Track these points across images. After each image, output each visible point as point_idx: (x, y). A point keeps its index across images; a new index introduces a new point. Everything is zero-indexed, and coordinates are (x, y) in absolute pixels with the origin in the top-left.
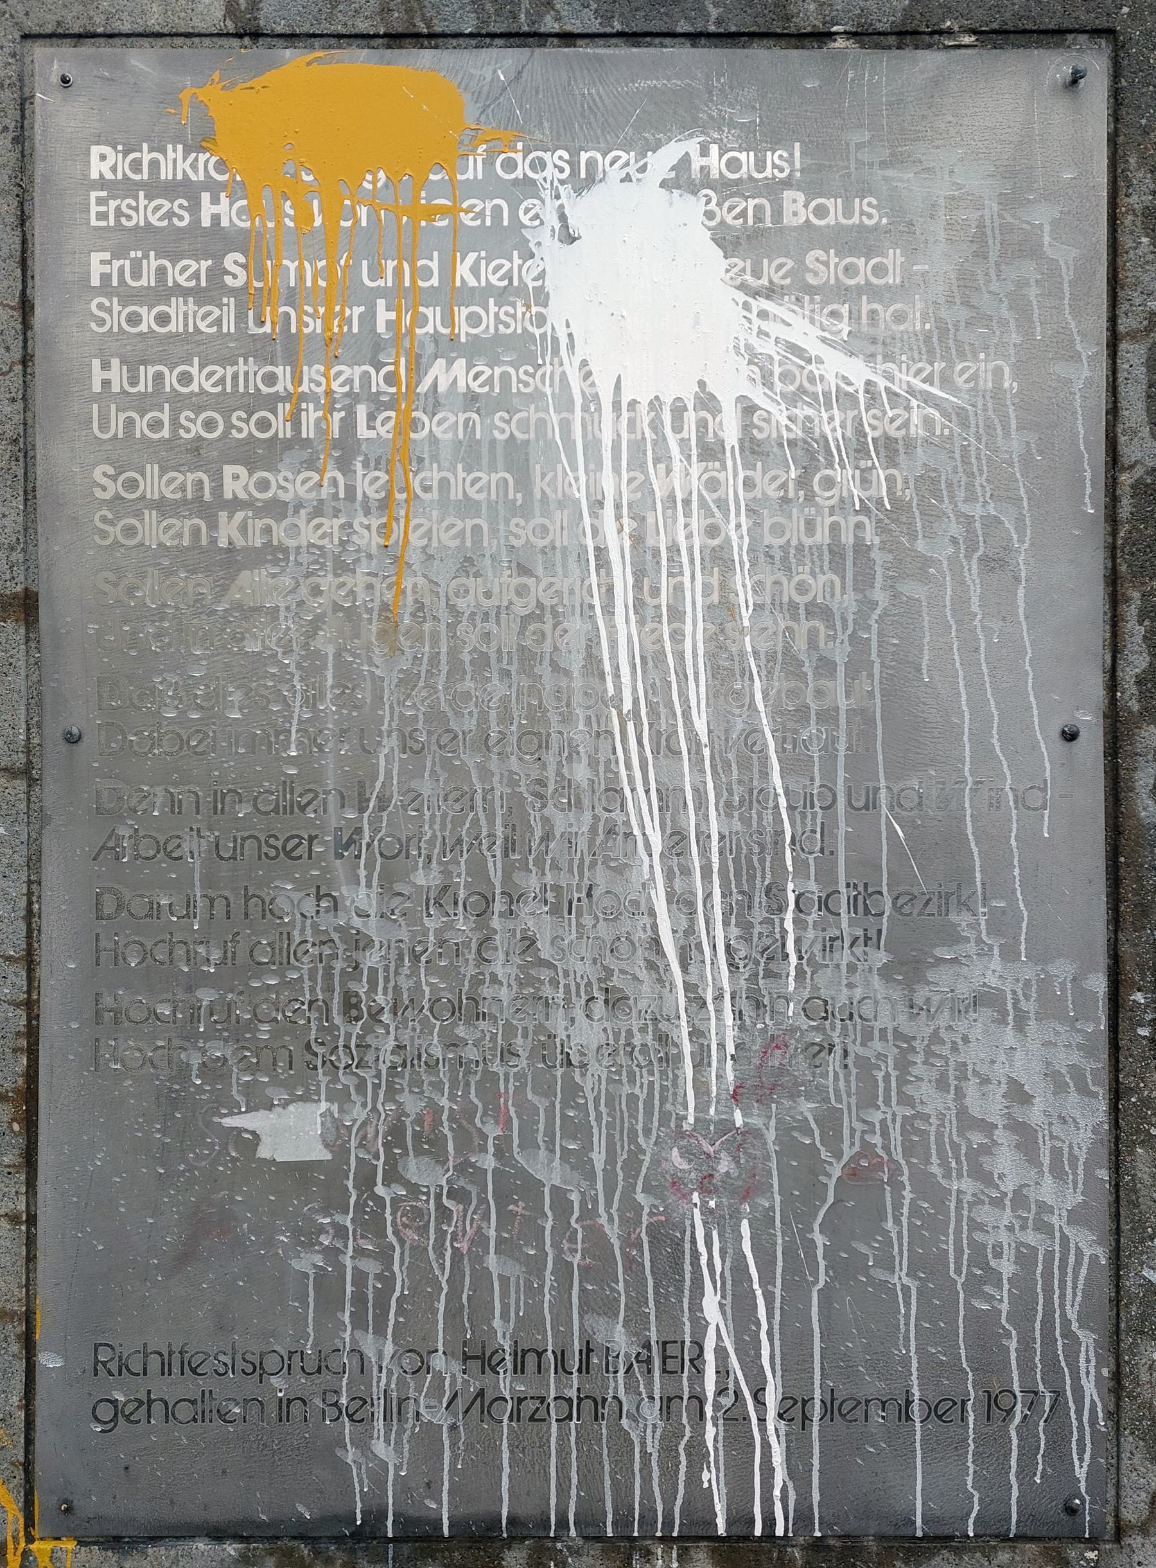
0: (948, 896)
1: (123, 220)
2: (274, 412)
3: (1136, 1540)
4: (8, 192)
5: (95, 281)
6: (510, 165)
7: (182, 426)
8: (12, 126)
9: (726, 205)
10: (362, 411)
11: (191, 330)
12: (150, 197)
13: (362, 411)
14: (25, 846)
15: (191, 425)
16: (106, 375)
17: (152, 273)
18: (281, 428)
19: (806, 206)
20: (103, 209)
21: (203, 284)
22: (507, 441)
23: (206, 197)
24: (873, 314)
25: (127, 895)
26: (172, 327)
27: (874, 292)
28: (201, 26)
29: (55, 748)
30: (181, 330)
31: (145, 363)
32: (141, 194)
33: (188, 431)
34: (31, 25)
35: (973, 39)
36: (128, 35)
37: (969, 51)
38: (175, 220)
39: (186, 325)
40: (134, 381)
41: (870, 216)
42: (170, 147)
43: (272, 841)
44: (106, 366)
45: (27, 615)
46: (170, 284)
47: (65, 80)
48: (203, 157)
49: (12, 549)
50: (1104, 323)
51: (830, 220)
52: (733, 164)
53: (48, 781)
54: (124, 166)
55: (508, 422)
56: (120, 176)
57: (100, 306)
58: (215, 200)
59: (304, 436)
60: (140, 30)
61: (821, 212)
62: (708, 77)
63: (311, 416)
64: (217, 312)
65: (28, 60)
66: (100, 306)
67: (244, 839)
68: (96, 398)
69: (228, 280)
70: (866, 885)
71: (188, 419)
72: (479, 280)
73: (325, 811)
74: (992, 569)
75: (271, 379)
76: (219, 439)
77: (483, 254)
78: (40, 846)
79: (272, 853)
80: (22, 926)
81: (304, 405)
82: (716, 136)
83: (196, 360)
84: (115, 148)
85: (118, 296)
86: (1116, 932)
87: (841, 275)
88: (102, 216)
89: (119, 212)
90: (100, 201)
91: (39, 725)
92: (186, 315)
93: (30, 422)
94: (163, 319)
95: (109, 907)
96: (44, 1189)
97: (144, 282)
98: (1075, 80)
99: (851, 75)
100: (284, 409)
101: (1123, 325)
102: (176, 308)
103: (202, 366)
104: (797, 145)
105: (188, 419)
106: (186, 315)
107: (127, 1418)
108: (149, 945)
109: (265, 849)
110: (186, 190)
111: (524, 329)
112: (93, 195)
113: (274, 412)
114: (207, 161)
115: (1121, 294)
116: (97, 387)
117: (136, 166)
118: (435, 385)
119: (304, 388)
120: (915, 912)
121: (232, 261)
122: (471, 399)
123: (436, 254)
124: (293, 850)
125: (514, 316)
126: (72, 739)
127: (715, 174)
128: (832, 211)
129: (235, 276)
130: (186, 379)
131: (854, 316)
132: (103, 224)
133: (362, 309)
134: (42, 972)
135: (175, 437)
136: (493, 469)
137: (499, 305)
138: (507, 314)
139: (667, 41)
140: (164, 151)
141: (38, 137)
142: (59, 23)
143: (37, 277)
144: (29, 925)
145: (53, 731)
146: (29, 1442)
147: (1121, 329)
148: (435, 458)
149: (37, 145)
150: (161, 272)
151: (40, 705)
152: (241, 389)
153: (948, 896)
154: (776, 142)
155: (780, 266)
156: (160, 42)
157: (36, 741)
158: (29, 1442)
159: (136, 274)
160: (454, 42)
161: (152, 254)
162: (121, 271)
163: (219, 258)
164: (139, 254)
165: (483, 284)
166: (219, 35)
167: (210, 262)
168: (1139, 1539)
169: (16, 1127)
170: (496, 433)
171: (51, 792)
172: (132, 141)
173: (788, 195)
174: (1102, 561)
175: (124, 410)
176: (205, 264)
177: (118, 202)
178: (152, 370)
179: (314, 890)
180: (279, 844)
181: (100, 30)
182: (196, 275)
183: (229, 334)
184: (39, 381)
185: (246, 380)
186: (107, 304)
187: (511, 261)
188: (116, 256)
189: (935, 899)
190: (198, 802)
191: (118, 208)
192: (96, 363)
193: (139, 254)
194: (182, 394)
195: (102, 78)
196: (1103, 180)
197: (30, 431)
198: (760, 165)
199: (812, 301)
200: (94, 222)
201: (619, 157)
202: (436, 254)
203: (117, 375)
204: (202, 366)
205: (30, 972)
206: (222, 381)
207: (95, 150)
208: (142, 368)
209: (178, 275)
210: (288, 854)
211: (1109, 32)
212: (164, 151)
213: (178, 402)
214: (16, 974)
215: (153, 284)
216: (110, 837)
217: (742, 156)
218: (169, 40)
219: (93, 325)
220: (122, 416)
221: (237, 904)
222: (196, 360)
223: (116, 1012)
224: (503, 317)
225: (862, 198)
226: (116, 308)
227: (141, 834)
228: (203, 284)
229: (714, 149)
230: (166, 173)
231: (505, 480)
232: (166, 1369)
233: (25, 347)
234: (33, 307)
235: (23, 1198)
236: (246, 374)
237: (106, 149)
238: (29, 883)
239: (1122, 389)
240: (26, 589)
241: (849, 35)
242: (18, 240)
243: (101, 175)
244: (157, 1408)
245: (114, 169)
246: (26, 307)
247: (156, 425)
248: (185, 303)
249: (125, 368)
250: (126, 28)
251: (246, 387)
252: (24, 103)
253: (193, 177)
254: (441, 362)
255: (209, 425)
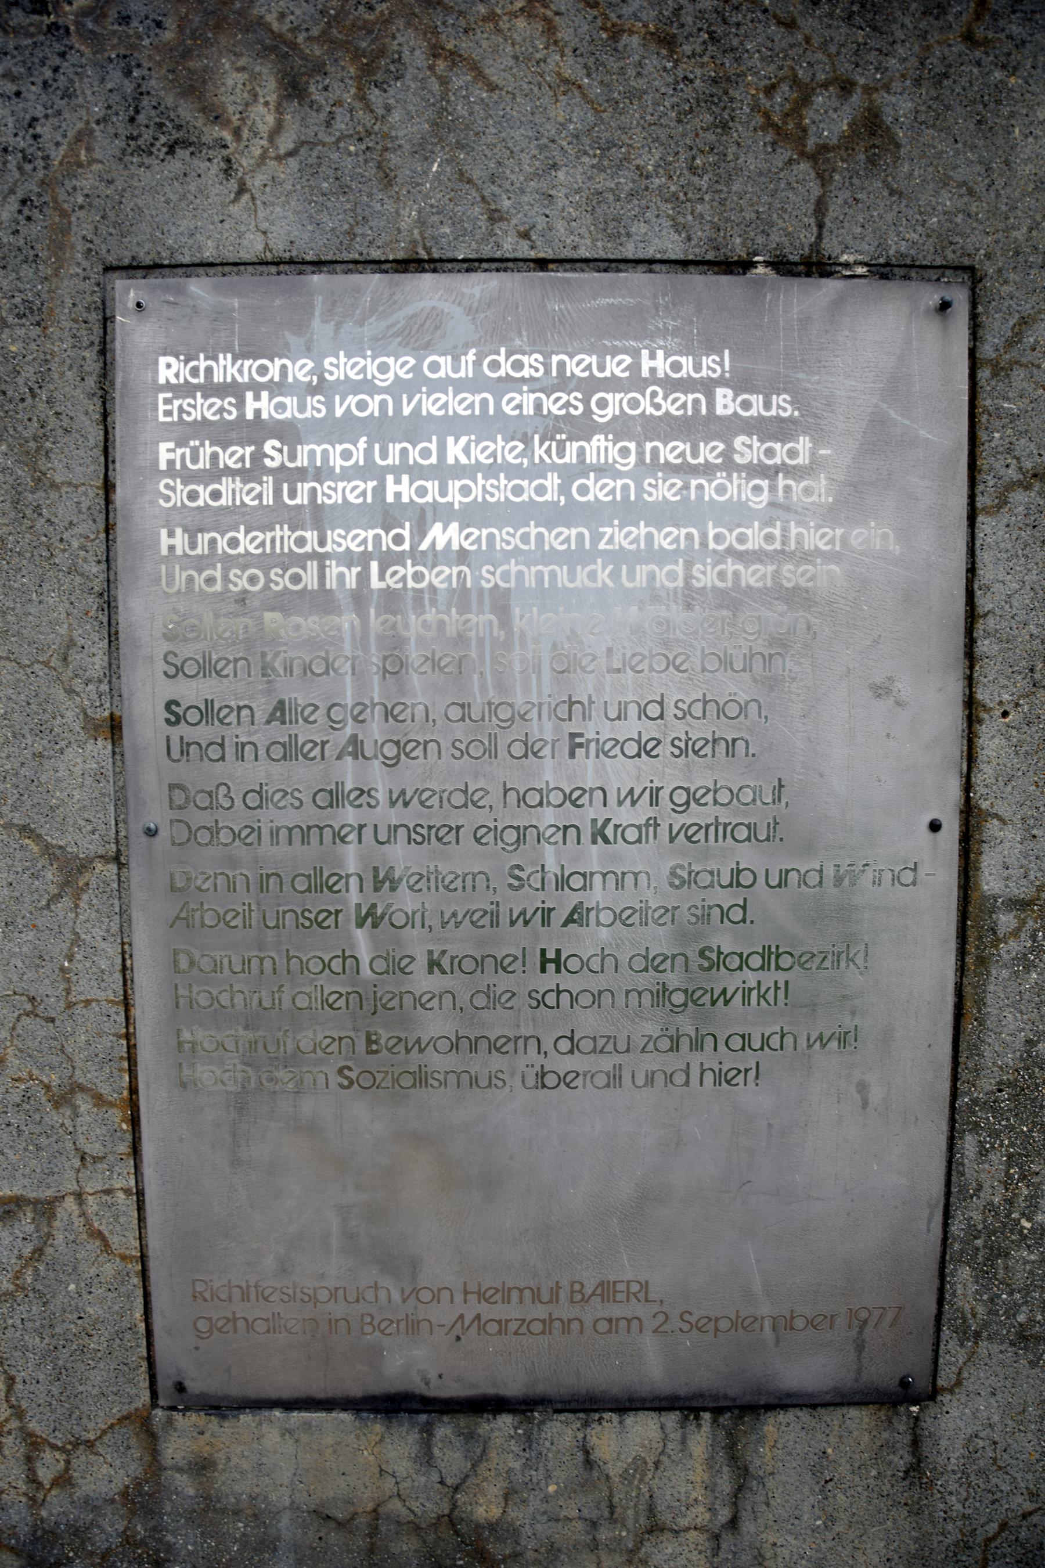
0: (839, 954)
1: (185, 416)
2: (304, 568)
3: (946, 1398)
4: (94, 395)
5: (163, 466)
6: (495, 366)
7: (231, 582)
8: (97, 342)
9: (671, 397)
10: (374, 565)
11: (238, 503)
12: (205, 397)
13: (374, 565)
14: (117, 917)
15: (238, 581)
16: (172, 541)
17: (208, 458)
18: (310, 578)
19: (734, 400)
20: (168, 407)
21: (248, 465)
22: (491, 589)
23: (249, 395)
24: (787, 489)
25: (197, 954)
26: (223, 502)
27: (790, 471)
28: (245, 256)
29: (138, 842)
30: (230, 503)
31: (201, 531)
32: (199, 394)
33: (236, 585)
34: (111, 259)
35: (865, 269)
36: (188, 266)
37: (862, 281)
38: (225, 415)
39: (234, 500)
40: (193, 545)
41: (785, 410)
42: (221, 356)
43: (307, 914)
44: (171, 534)
45: (113, 734)
46: (221, 466)
47: (139, 305)
48: (247, 363)
49: (100, 681)
50: (964, 501)
51: (753, 412)
52: (676, 367)
53: (133, 864)
54: (185, 373)
55: (493, 574)
56: (182, 381)
57: (167, 486)
58: (257, 398)
59: (328, 587)
60: (198, 261)
61: (746, 405)
62: (655, 297)
63: (334, 570)
64: (258, 488)
65: (109, 287)
66: (167, 486)
67: (285, 912)
68: (165, 560)
69: (267, 462)
70: (777, 947)
71: (236, 575)
72: (469, 458)
73: (347, 890)
74: (879, 696)
75: (301, 542)
76: (261, 592)
77: (473, 437)
78: (129, 916)
79: (307, 924)
80: (118, 976)
81: (328, 563)
82: (662, 343)
83: (242, 528)
84: (177, 358)
85: (181, 477)
86: (961, 977)
87: (762, 457)
88: (168, 413)
89: (181, 410)
90: (167, 401)
91: (125, 822)
92: (234, 491)
93: (112, 578)
94: (216, 495)
95: (184, 964)
96: (149, 1172)
97: (201, 466)
98: (945, 306)
99: (768, 297)
100: (313, 566)
101: (981, 501)
102: (226, 486)
103: (247, 532)
104: (727, 352)
105: (236, 575)
106: (234, 491)
107: (219, 1330)
108: (215, 992)
109: (301, 920)
110: (234, 390)
111: (507, 498)
112: (161, 396)
113: (304, 568)
114: (250, 367)
115: (979, 477)
116: (164, 551)
117: (195, 372)
118: (433, 544)
119: (328, 548)
120: (814, 967)
121: (270, 446)
122: (463, 556)
123: (434, 438)
124: (681, 664)
125: (498, 488)
126: (151, 833)
127: (661, 374)
128: (755, 404)
129: (273, 459)
130: (234, 543)
131: (773, 488)
132: (169, 419)
133: (375, 483)
134: (136, 1012)
135: (226, 590)
136: (483, 612)
137: (486, 478)
138: (492, 486)
139: (622, 266)
140: (216, 359)
141: (118, 352)
142: (133, 258)
143: (118, 464)
144: (124, 976)
145: (136, 828)
146: (150, 1345)
147: (979, 505)
148: (433, 602)
149: (118, 358)
150: (214, 457)
151: (125, 804)
152: (278, 550)
153: (839, 954)
154: (711, 347)
155: (714, 448)
156: (212, 271)
157: (122, 834)
158: (150, 1345)
159: (195, 459)
160: (449, 266)
161: (207, 443)
162: (183, 456)
163: (259, 444)
164: (197, 443)
165: (473, 461)
166: (260, 264)
167: (253, 448)
168: (949, 1397)
169: (124, 1126)
170: (484, 583)
171: (136, 874)
172: (192, 352)
173: (720, 392)
174: (961, 689)
175: (186, 569)
176: (249, 450)
177: (180, 401)
178: (207, 536)
179: (340, 953)
180: (312, 916)
181: (166, 262)
182: (242, 459)
183: (268, 506)
184: (120, 546)
185: (282, 543)
186: (172, 483)
187: (495, 442)
188: (179, 445)
189: (830, 957)
190: (248, 883)
191: (180, 408)
192: (164, 532)
193: (197, 443)
194: (230, 556)
195: (169, 302)
196: (965, 387)
197: (112, 586)
198: (697, 368)
199: (739, 477)
200: (162, 418)
201: (583, 360)
202: (434, 438)
203: (180, 540)
204: (247, 532)
205: (127, 1011)
206: (263, 544)
207: (163, 360)
208: (200, 535)
209: (228, 458)
210: (319, 925)
211: (971, 269)
212: (216, 359)
213: (228, 561)
214: (117, 1013)
215: (208, 467)
216: (181, 910)
217: (683, 360)
218: (220, 268)
219: (161, 502)
220: (185, 574)
221: (281, 962)
222: (242, 528)
223: (194, 1044)
224: (489, 488)
225: (779, 395)
226: (179, 487)
227: (206, 907)
228: (248, 465)
229: (660, 354)
230: (218, 377)
231: (491, 622)
232: (245, 1297)
233: (107, 519)
234: (114, 486)
235: (133, 1177)
236: (282, 538)
237: (171, 360)
238: (123, 944)
239: (978, 552)
240: (112, 714)
241: (767, 264)
242: (102, 433)
243: (167, 381)
244: (241, 1324)
245: (177, 375)
246: (108, 487)
247: (210, 581)
248: (234, 481)
249: (186, 536)
250: (187, 260)
251: (282, 548)
252: (107, 321)
253: (240, 379)
254: (438, 526)
255: (253, 580)
